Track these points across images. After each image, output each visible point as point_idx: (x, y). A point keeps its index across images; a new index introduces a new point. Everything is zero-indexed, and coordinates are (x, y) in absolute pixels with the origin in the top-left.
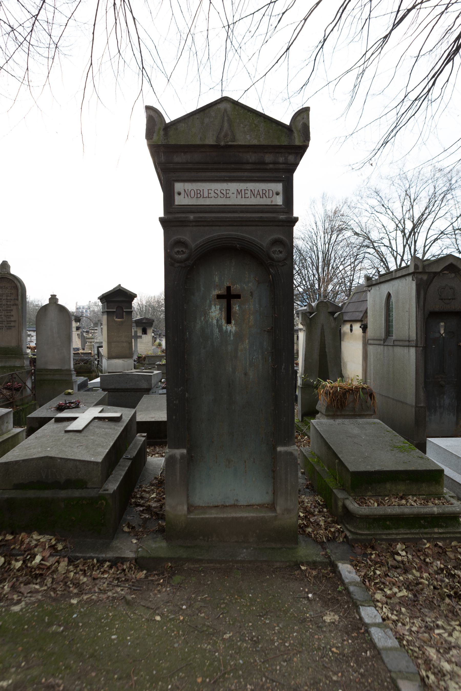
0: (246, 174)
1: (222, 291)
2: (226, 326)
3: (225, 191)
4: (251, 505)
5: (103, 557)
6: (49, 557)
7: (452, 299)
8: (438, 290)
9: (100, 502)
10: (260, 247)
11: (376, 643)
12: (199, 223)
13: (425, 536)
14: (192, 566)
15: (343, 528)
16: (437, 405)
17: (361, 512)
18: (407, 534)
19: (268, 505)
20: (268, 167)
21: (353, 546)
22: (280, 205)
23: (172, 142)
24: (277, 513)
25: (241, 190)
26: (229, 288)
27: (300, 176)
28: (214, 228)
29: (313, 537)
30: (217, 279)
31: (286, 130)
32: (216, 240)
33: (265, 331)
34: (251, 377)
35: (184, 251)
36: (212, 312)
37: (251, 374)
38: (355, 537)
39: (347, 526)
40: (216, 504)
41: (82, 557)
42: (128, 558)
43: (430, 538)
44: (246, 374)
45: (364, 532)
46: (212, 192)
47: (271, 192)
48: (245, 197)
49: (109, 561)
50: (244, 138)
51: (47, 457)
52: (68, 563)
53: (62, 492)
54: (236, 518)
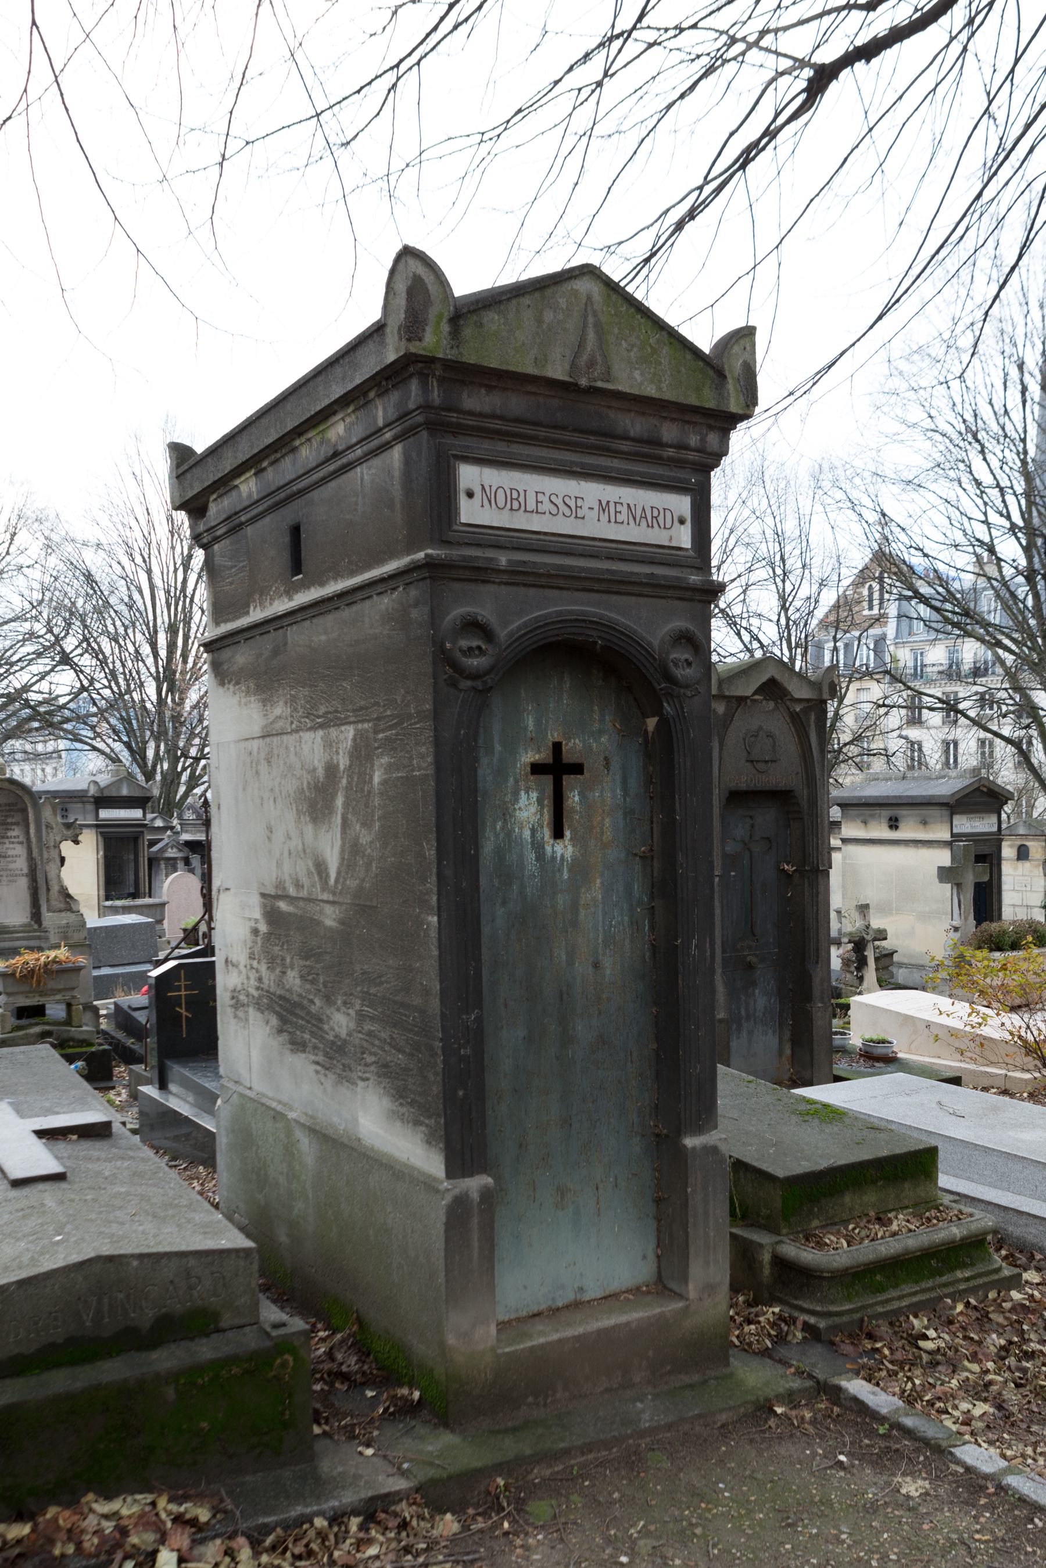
0: (616, 463)
1: (543, 756)
2: (553, 846)
3: (574, 499)
4: (610, 1296)
5: (333, 1508)
6: (191, 1548)
7: (772, 761)
8: (744, 739)
9: (279, 1361)
10: (646, 650)
11: (1036, 1502)
12: (520, 577)
13: (946, 1291)
14: (547, 1472)
15: (787, 1309)
16: (743, 1013)
17: (835, 1264)
18: (915, 1294)
19: (647, 1286)
20: (665, 454)
21: (832, 1343)
22: (687, 550)
23: (470, 356)
24: (687, 1299)
25: (608, 502)
26: (557, 747)
27: (726, 485)
28: (548, 592)
29: (737, 1343)
30: (530, 723)
31: (711, 372)
32: (553, 623)
33: (636, 855)
34: (608, 972)
35: (484, 647)
36: (520, 809)
37: (607, 964)
38: (831, 1321)
39: (800, 1303)
40: (535, 1309)
41: (277, 1524)
42: (398, 1493)
43: (955, 1292)
44: (596, 965)
45: (843, 1308)
46: (546, 500)
47: (668, 514)
48: (616, 522)
49: (355, 1513)
50: (631, 378)
51: (98, 1259)
52: (253, 1548)
53: (155, 1355)
54: (606, 1331)
